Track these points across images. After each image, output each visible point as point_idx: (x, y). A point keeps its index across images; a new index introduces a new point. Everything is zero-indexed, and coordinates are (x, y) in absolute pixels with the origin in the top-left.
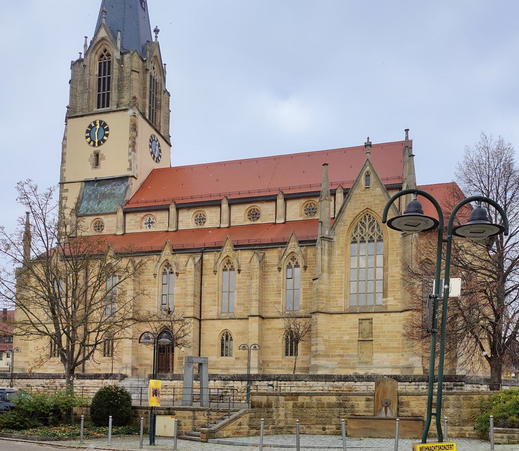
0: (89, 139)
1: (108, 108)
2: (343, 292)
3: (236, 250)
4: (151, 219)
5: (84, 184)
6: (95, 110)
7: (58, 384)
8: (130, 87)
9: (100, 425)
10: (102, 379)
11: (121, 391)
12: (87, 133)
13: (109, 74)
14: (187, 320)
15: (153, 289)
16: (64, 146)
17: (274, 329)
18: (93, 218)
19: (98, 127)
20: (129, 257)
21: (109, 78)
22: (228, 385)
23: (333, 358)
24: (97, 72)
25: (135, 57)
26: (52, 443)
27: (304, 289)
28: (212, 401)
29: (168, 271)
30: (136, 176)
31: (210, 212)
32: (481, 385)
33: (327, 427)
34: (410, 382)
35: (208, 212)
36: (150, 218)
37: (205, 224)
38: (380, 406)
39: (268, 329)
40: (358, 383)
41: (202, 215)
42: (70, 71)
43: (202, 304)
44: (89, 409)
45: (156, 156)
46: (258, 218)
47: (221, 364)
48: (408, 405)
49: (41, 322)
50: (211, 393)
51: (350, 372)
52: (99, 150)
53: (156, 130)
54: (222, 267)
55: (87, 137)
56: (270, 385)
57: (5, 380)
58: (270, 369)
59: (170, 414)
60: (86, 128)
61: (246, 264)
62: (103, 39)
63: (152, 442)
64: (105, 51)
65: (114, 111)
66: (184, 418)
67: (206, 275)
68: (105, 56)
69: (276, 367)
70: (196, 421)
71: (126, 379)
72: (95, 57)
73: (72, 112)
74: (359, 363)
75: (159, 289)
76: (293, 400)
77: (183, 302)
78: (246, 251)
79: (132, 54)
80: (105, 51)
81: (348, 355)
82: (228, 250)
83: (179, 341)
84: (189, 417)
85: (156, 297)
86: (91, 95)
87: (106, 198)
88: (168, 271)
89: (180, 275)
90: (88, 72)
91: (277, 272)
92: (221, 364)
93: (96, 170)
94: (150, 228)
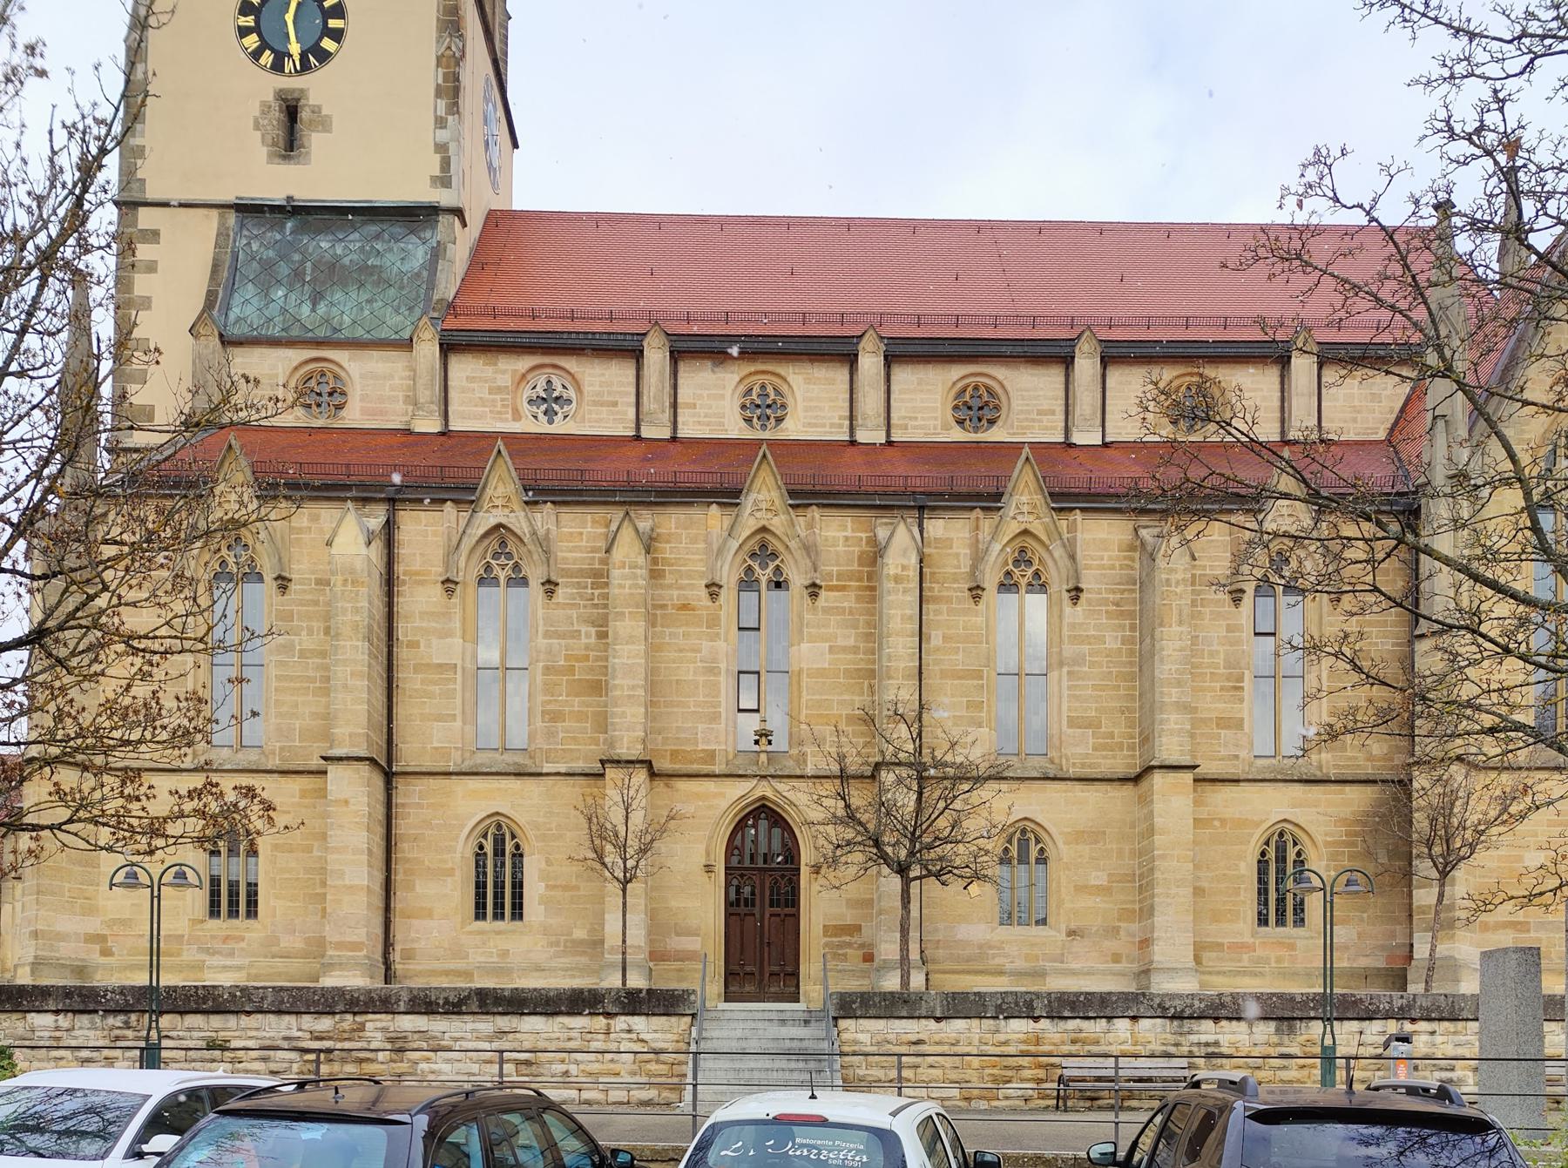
0: (252, 41)
3: (1061, 510)
4: (557, 383)
5: (232, 218)
7: (379, 1035)
10: (608, 1015)
15: (706, 645)
17: (1217, 823)
18: (296, 355)
22: (1194, 1038)
28: (1126, 1104)
29: (764, 575)
31: (808, 381)
35: (800, 378)
36: (549, 382)
37: (786, 424)
41: (770, 390)
46: (992, 422)
47: (1006, 956)
49: (1443, 624)
50: (1121, 1073)
52: (302, 91)
55: (243, 32)
57: (84, 1020)
58: (1210, 973)
61: (1102, 567)
67: (936, 600)
77: (841, 703)
78: (1104, 516)
82: (1025, 509)
87: (343, 283)
88: (764, 575)
89: (823, 593)
91: (1228, 607)
92: (1006, 956)
94: (551, 422)
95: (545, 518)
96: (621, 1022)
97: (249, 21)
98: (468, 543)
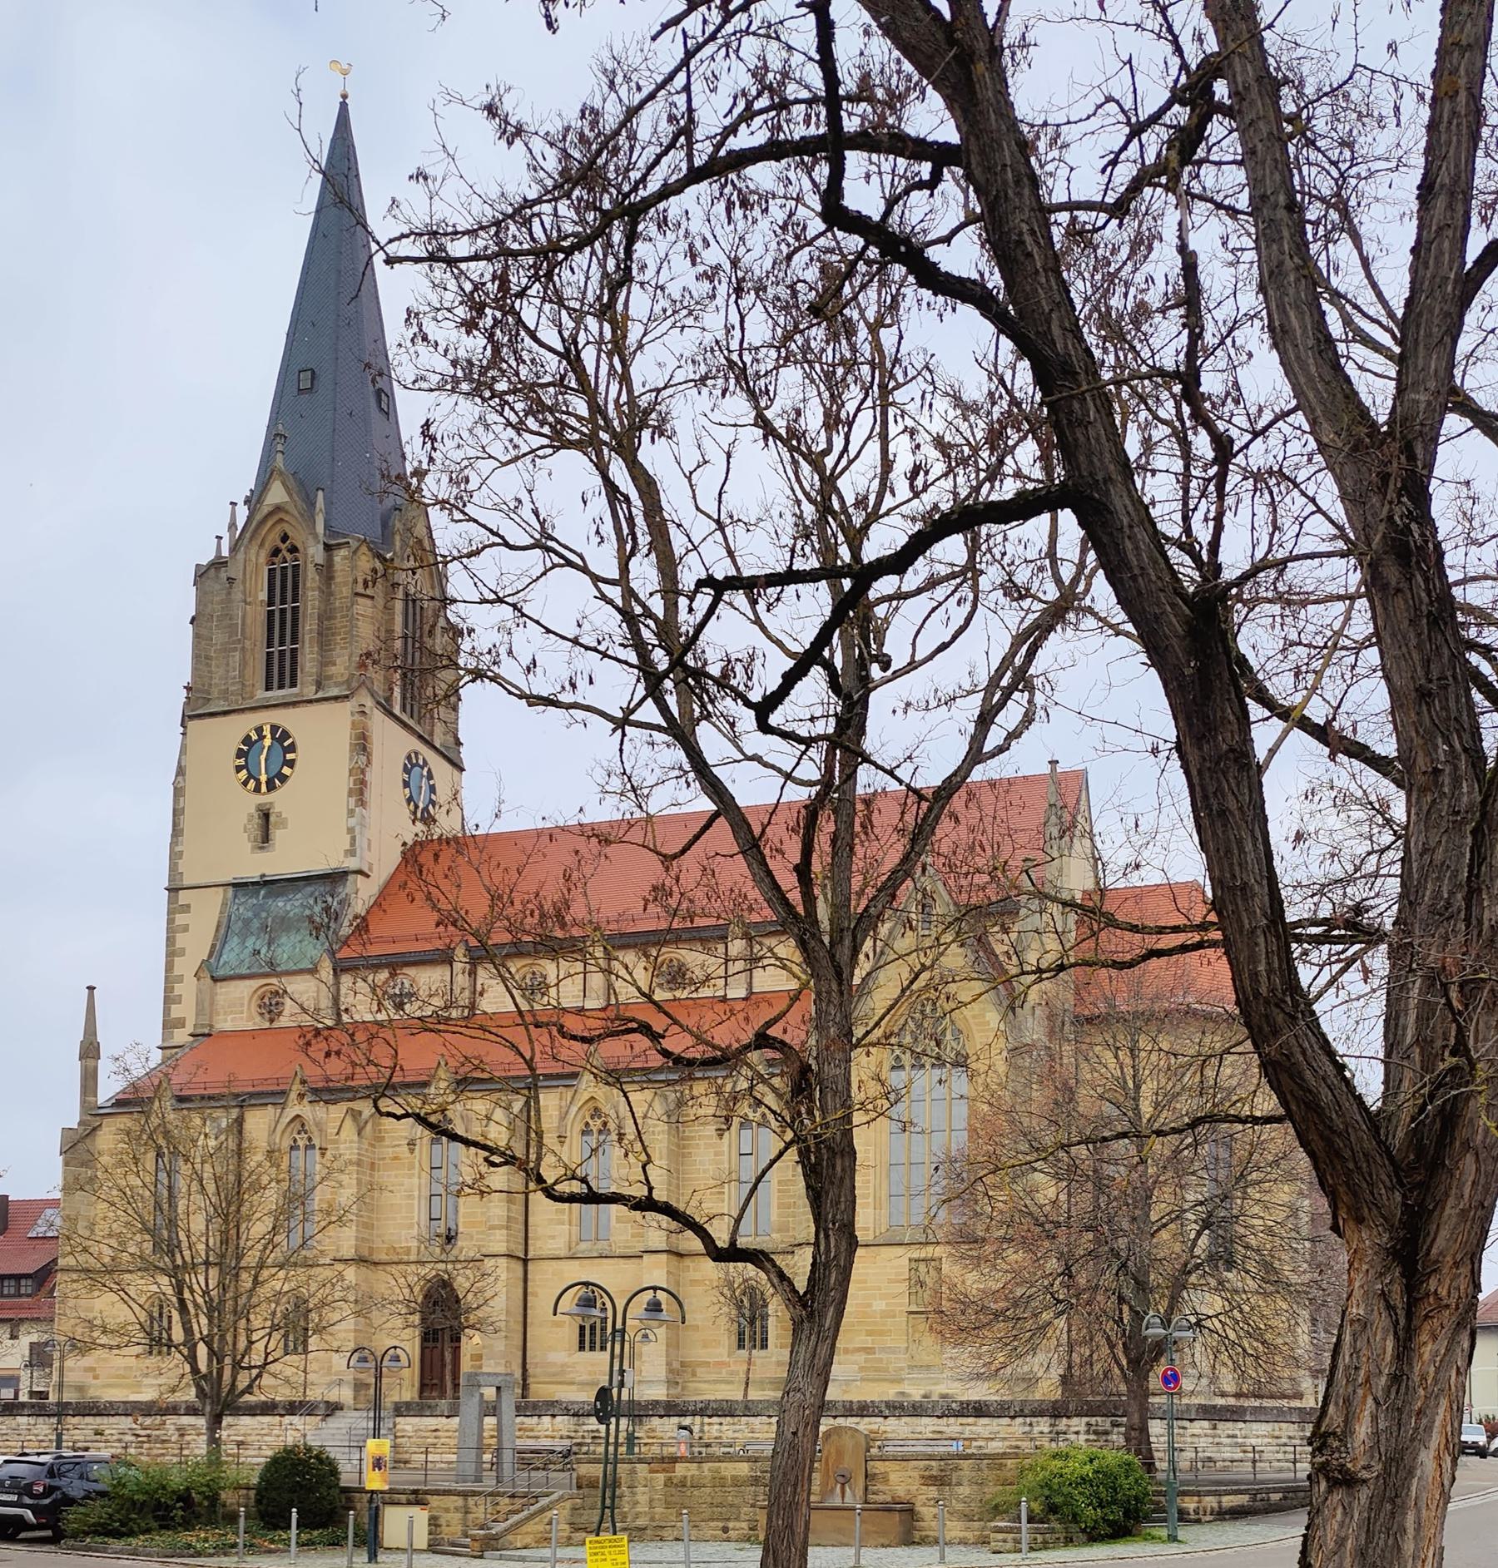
0: (243, 774)
1: (294, 690)
2: (871, 1191)
5: (231, 890)
6: (261, 694)
8: (351, 636)
9: (276, 1527)
10: (282, 1416)
11: (317, 1457)
12: (238, 757)
13: (295, 600)
14: (489, 1263)
15: (406, 1181)
16: (178, 792)
18: (255, 983)
19: (267, 742)
20: (342, 1100)
21: (295, 610)
22: (585, 1428)
23: (849, 1357)
24: (263, 596)
25: (363, 558)
26: (186, 1561)
27: (779, 1182)
30: (366, 870)
32: (1191, 1420)
33: (731, 1525)
34: (1013, 1418)
38: (832, 1481)
39: (694, 1282)
40: (891, 1420)
42: (193, 590)
43: (530, 1219)
44: (252, 1493)
45: (421, 805)
48: (886, 1480)
51: (889, 1392)
53: (420, 737)
54: (579, 1126)
55: (239, 769)
56: (684, 1428)
57: (41, 1419)
59: (418, 1503)
60: (236, 743)
62: (278, 509)
63: (373, 1557)
64: (285, 538)
65: (310, 701)
66: (447, 1510)
68: (284, 552)
69: (713, 1377)
70: (470, 1516)
71: (339, 1413)
72: (258, 555)
73: (200, 702)
74: (911, 1367)
75: (423, 1181)
76: (664, 1470)
79: (355, 552)
80: (285, 538)
81: (883, 1350)
83: (472, 1318)
84: (456, 1509)
85: (416, 1202)
86: (248, 654)
87: (288, 930)
90: (240, 596)
91: (716, 1140)
96: (287, 1419)
97: (242, 762)
98: (280, 1127)
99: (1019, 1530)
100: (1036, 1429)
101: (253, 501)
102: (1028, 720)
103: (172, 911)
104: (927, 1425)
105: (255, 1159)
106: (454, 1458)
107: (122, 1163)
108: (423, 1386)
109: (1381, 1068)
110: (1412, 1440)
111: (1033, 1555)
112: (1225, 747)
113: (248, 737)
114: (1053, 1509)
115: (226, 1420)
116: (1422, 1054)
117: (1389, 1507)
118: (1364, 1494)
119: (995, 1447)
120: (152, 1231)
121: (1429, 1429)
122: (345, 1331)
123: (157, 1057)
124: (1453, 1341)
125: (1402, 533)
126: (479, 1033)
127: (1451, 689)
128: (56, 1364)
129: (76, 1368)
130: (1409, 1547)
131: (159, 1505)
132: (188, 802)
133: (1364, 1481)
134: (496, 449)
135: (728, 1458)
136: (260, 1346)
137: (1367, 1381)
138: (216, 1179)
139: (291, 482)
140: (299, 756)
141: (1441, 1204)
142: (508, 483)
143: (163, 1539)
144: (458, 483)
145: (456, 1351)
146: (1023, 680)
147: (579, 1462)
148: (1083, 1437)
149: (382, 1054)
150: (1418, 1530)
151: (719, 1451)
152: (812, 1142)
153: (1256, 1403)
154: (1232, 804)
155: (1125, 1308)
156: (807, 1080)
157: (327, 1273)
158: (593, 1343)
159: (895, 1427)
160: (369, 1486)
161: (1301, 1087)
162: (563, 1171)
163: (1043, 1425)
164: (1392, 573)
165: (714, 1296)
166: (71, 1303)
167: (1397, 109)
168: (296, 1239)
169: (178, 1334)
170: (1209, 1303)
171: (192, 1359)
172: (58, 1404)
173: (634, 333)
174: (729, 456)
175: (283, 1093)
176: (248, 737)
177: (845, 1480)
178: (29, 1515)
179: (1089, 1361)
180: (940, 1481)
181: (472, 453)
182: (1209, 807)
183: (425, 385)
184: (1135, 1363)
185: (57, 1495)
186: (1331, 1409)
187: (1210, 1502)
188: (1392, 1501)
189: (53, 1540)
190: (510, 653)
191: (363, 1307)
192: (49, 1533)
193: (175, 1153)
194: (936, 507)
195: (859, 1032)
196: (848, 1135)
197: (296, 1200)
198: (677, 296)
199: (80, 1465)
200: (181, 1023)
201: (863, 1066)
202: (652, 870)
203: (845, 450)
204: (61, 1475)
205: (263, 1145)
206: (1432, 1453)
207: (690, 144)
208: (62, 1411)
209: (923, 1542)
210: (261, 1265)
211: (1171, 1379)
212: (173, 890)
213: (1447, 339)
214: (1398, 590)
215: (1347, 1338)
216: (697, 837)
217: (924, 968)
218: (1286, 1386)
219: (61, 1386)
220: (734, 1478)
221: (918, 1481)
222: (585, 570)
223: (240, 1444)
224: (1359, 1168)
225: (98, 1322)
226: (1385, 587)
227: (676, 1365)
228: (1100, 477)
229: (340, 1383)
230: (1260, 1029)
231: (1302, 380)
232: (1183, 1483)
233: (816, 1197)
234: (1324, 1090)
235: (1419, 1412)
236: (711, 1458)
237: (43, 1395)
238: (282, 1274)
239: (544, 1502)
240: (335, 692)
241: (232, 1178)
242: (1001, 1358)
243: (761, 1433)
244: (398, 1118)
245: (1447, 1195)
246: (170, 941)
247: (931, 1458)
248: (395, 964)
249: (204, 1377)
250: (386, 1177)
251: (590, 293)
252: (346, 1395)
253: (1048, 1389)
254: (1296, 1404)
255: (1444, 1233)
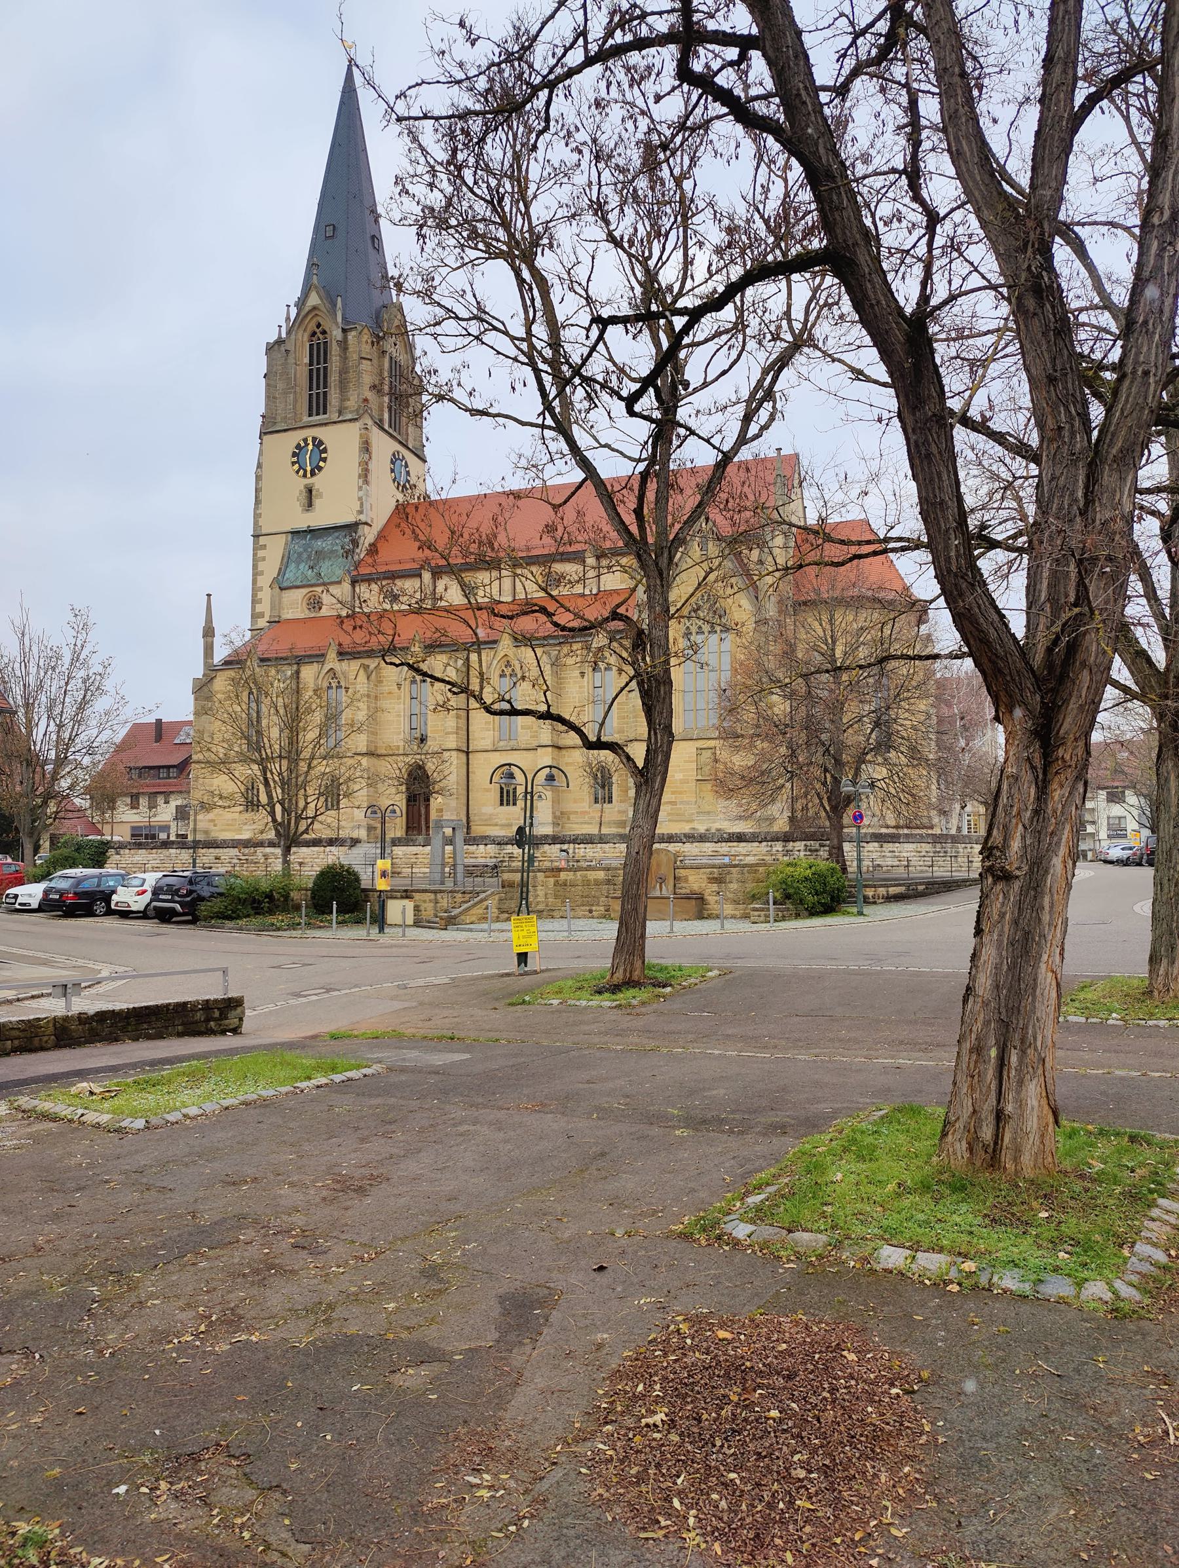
0: (296, 467)
6: (306, 419)
8: (359, 384)
9: (323, 913)
13: (325, 362)
14: (446, 755)
15: (396, 706)
16: (258, 478)
18: (305, 591)
19: (310, 447)
21: (325, 368)
24: (307, 360)
40: (687, 845)
42: (264, 359)
48: (686, 881)
51: (686, 828)
53: (400, 443)
54: (498, 672)
55: (293, 463)
59: (407, 897)
60: (292, 448)
62: (314, 308)
63: (381, 930)
64: (319, 325)
65: (335, 423)
66: (425, 901)
80: (319, 325)
81: (682, 803)
83: (437, 788)
84: (430, 901)
91: (580, 679)
93: (309, 514)
95: (345, 664)
96: (328, 849)
98: (321, 676)
99: (768, 910)
100: (774, 849)
101: (300, 303)
102: (772, 418)
103: (255, 549)
104: (709, 847)
105: (307, 694)
106: (427, 870)
107: (230, 698)
108: (408, 828)
109: (1024, 616)
110: (1047, 851)
111: (777, 924)
112: (930, 414)
113: (299, 444)
114: (788, 896)
115: (293, 850)
116: (1051, 607)
117: (1033, 893)
118: (1017, 885)
119: (750, 860)
120: (247, 738)
121: (1058, 844)
122: (362, 796)
123: (248, 634)
124: (1073, 788)
125: (1037, 277)
126: (445, 614)
127: (1069, 376)
128: (192, 818)
129: (203, 820)
130: (1046, 918)
131: (254, 901)
132: (264, 484)
133: (1017, 877)
134: (451, 261)
135: (589, 868)
136: (312, 805)
137: (1019, 814)
138: (285, 707)
139: (322, 292)
140: (328, 455)
141: (1066, 702)
142: (459, 279)
143: (257, 921)
144: (427, 281)
145: (427, 807)
146: (769, 395)
147: (503, 872)
148: (802, 853)
149: (387, 627)
150: (1051, 907)
151: (584, 864)
152: (645, 676)
153: (906, 831)
154: (934, 449)
155: (828, 775)
156: (641, 639)
157: (350, 762)
158: (508, 801)
159: (690, 849)
160: (379, 888)
161: (977, 629)
162: (496, 696)
163: (778, 846)
164: (1030, 303)
165: (581, 772)
166: (201, 781)
167: (1016, 22)
168: (332, 742)
169: (264, 799)
170: (879, 772)
171: (272, 813)
172: (194, 841)
173: (532, 188)
174: (593, 258)
175: (323, 655)
176: (299, 444)
177: (662, 880)
178: (178, 907)
179: (805, 808)
180: (719, 880)
181: (436, 263)
182: (919, 452)
183: (406, 222)
184: (834, 808)
185: (195, 895)
186: (995, 832)
187: (882, 891)
188: (1035, 889)
189: (194, 922)
190: (459, 384)
191: (373, 781)
192: (190, 918)
193: (259, 689)
194: (715, 291)
195: (672, 610)
196: (667, 672)
197: (332, 718)
198: (557, 165)
199: (207, 878)
200: (262, 615)
201: (675, 630)
202: (547, 514)
203: (660, 258)
204: (196, 883)
205: (312, 685)
206: (1060, 859)
207: (586, 42)
208: (196, 845)
209: (709, 917)
210: (312, 758)
211: (859, 817)
212: (256, 536)
213: (1063, 156)
214: (1035, 314)
215: (1005, 787)
216: (573, 494)
217: (712, 570)
218: (925, 821)
219: (195, 830)
220: (595, 880)
221: (706, 881)
222: (506, 333)
223: (301, 864)
224: (1014, 680)
225: (217, 792)
226: (1026, 312)
227: (558, 814)
228: (850, 243)
229: (359, 827)
230: (951, 593)
231: (971, 184)
232: (866, 880)
233: (649, 710)
234: (992, 631)
235: (1052, 834)
236: (580, 869)
237: (185, 836)
238: (325, 762)
239: (482, 896)
240: (349, 416)
241: (294, 706)
242: (754, 806)
243: (615, 853)
244: (397, 666)
245: (1071, 695)
246: (255, 567)
247: (713, 867)
248: (393, 576)
249: (280, 824)
250: (384, 704)
251: (506, 163)
252: (362, 834)
253: (781, 825)
254: (930, 832)
255: (1068, 720)
